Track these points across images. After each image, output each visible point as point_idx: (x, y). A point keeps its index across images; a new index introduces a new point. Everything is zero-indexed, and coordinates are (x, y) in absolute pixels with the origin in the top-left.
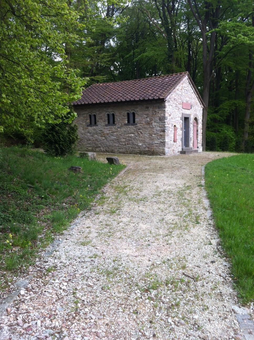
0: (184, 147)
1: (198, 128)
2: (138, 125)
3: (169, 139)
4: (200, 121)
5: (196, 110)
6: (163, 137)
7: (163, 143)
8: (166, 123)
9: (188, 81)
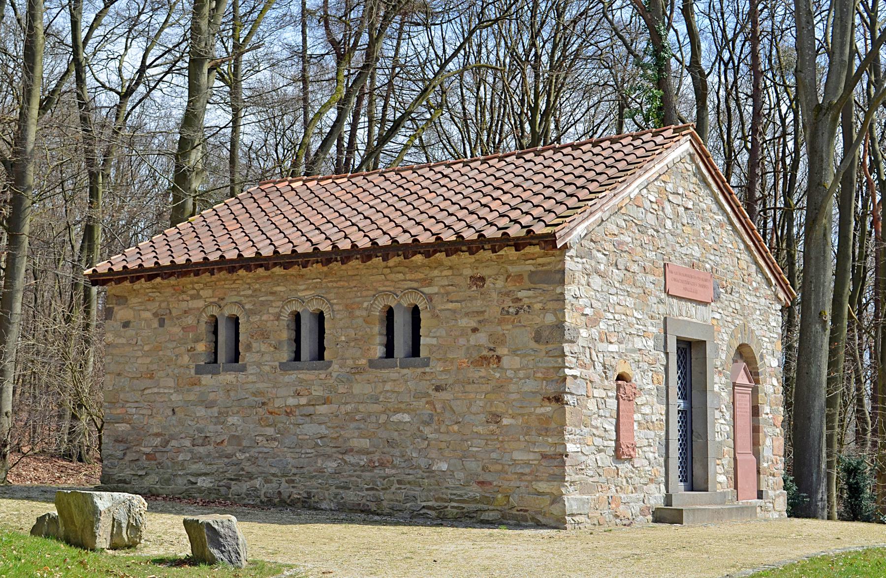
0: (678, 487)
1: (761, 395)
2: (437, 367)
3: (584, 444)
4: (772, 361)
5: (743, 312)
8: (570, 360)
9: (691, 167)
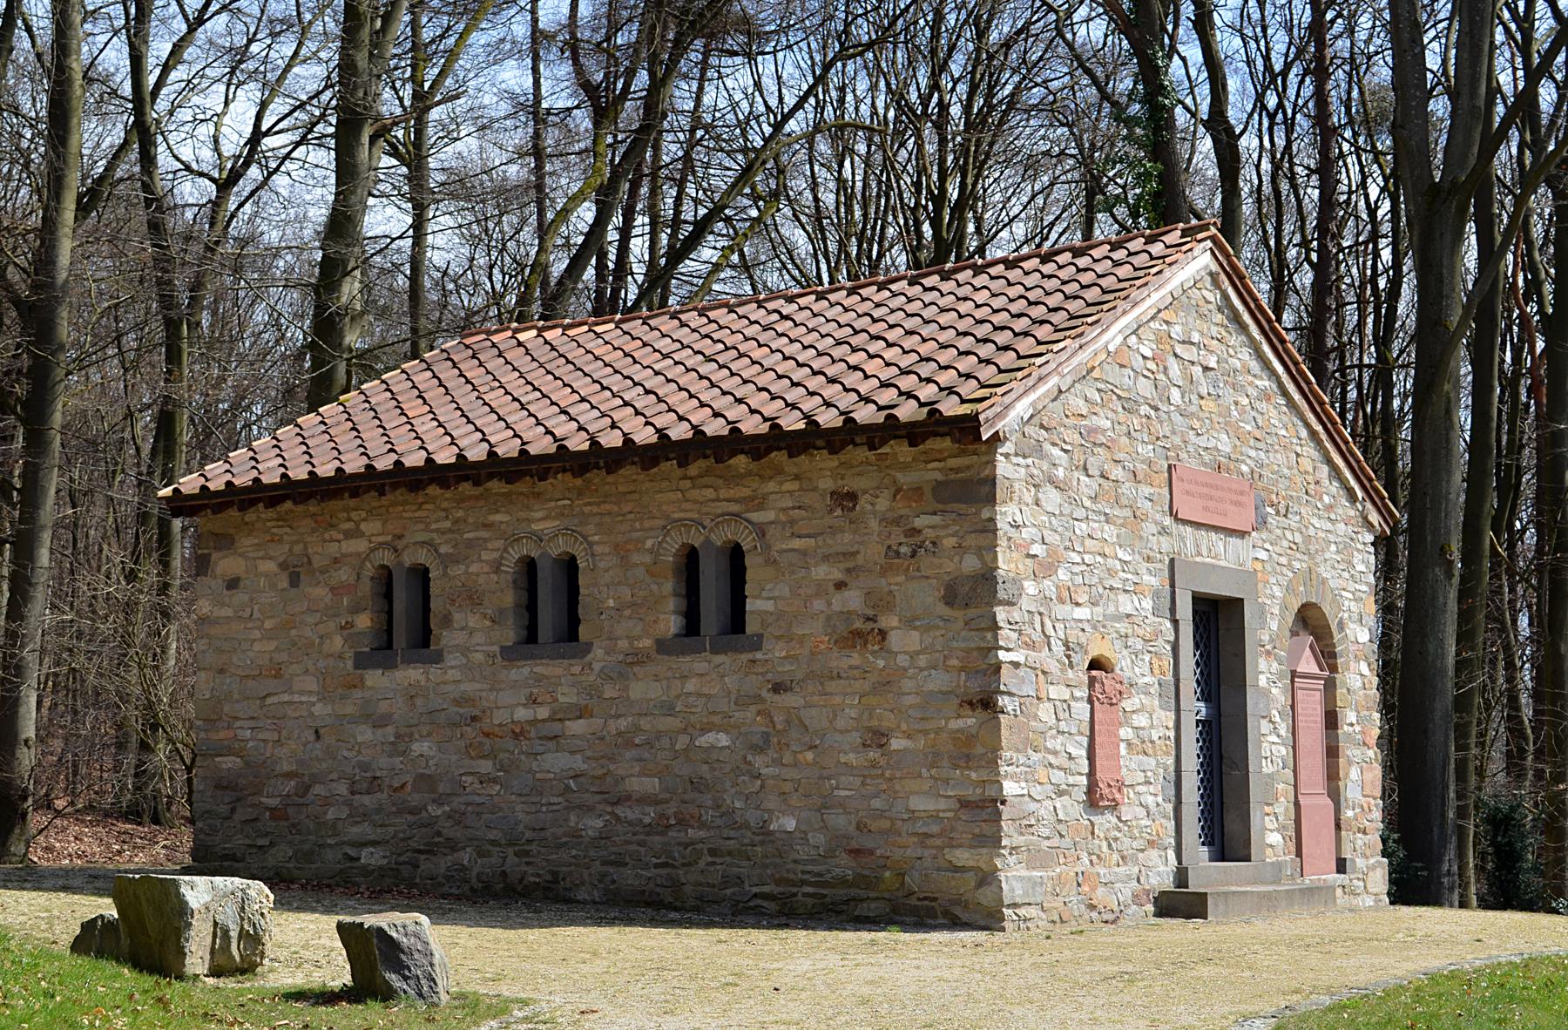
5: (1306, 547)
6: (980, 753)
7: (985, 810)
8: (1006, 635)
9: (1213, 297)
